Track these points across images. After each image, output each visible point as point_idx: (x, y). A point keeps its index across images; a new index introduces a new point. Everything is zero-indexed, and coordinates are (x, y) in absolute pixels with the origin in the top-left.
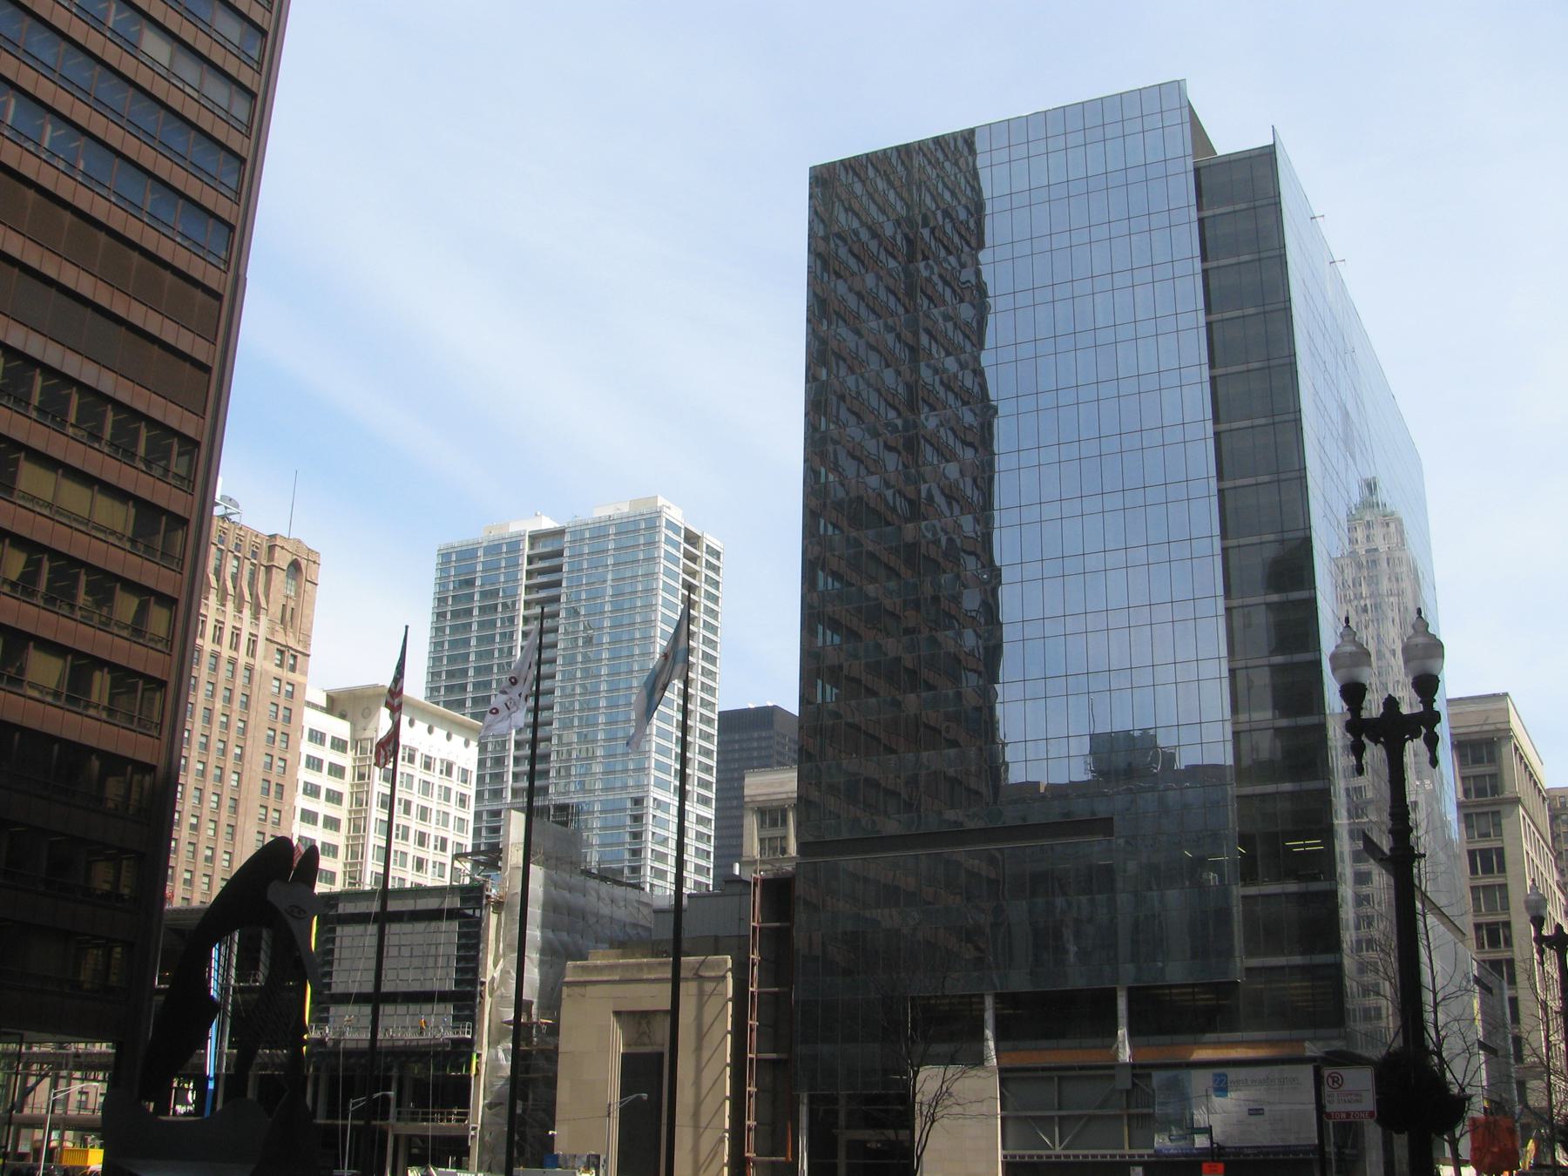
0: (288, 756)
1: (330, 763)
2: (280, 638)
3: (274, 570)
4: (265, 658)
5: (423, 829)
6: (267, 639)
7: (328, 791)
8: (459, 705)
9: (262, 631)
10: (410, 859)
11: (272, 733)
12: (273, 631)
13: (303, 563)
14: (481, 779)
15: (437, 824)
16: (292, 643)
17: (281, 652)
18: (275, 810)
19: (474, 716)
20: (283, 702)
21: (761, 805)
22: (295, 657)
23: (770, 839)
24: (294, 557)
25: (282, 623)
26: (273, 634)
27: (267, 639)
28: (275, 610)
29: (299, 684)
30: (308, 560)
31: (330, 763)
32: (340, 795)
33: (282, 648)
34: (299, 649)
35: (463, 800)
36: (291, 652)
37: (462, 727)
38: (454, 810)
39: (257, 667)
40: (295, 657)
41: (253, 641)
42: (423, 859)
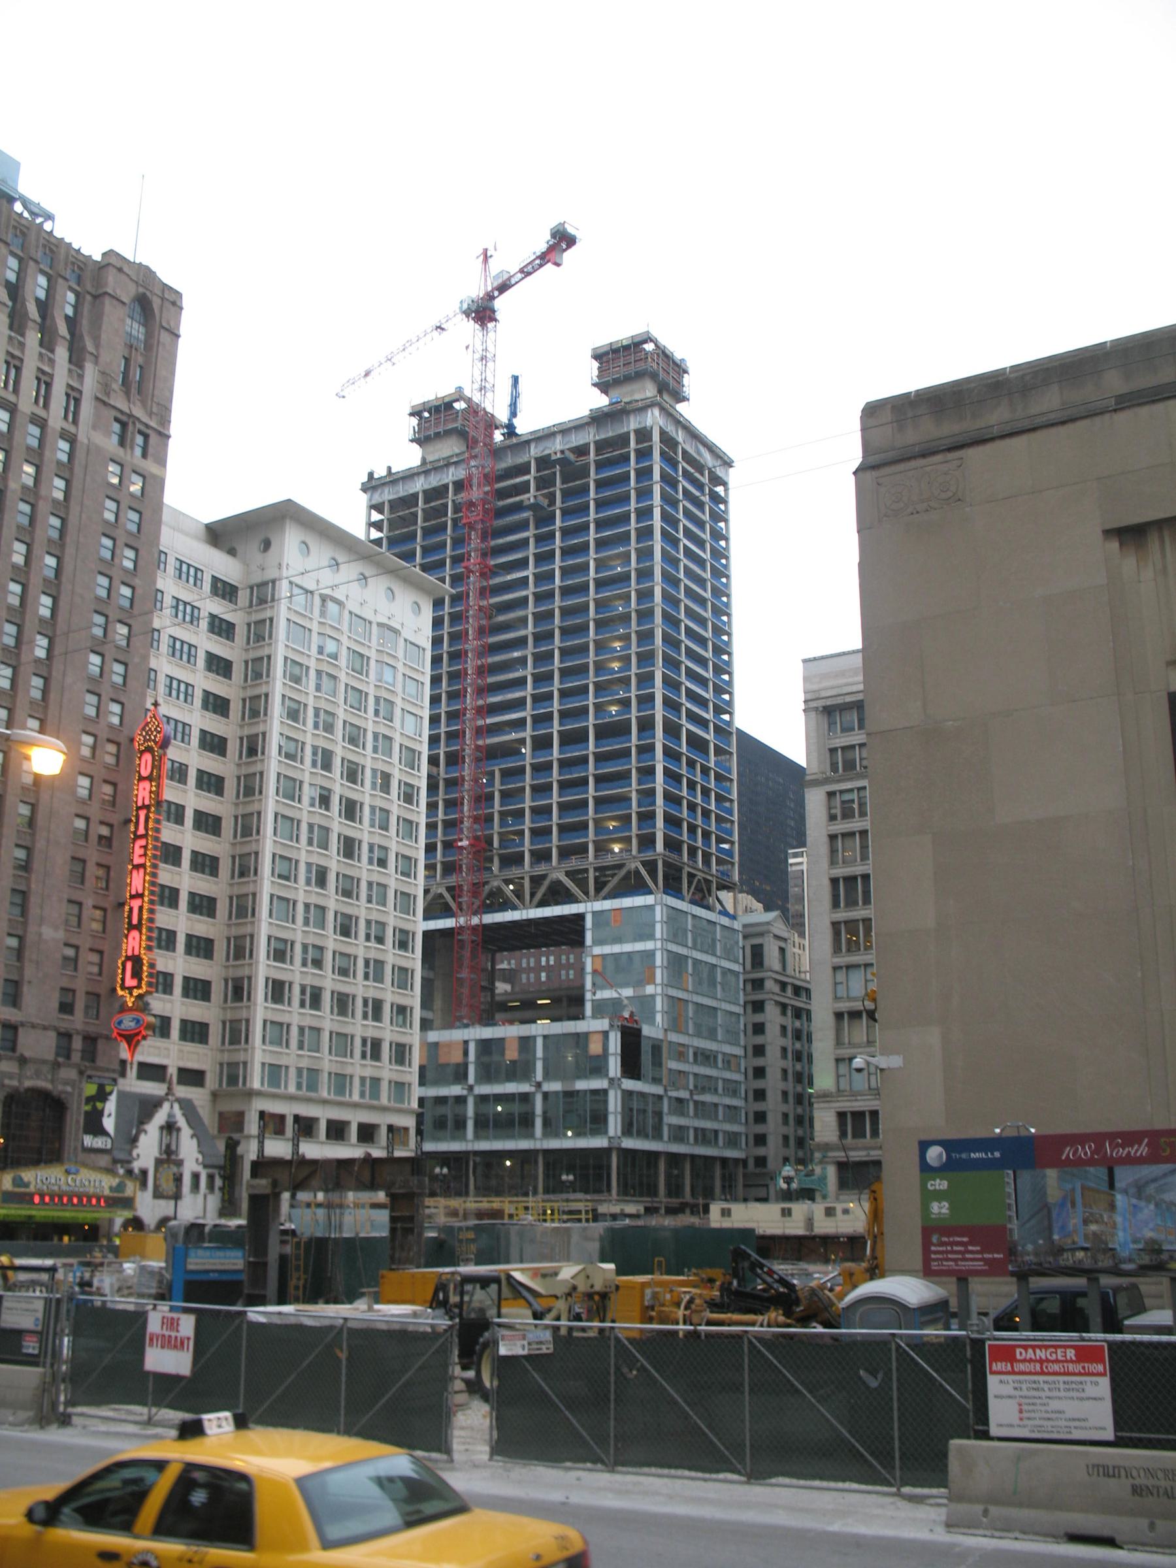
0: (137, 582)
1: (196, 811)
2: (120, 402)
3: (107, 301)
4: (94, 427)
5: (354, 796)
6: (97, 398)
7: (201, 773)
8: (409, 557)
9: (90, 383)
10: (334, 839)
11: (70, 952)
12: (106, 388)
13: (156, 303)
14: (433, 761)
15: (372, 826)
16: (138, 412)
17: (124, 425)
18: (91, 950)
19: (425, 568)
20: (93, 855)
21: (829, 702)
22: (146, 437)
23: (843, 748)
24: (141, 290)
25: (123, 383)
26: (108, 394)
27: (97, 398)
28: (113, 359)
29: (154, 477)
30: (163, 299)
31: (196, 811)
32: (217, 820)
33: (124, 418)
34: (153, 424)
35: (409, 797)
36: (138, 426)
37: (408, 581)
38: (391, 955)
39: (82, 438)
40: (146, 437)
41: (74, 397)
42: (347, 995)
